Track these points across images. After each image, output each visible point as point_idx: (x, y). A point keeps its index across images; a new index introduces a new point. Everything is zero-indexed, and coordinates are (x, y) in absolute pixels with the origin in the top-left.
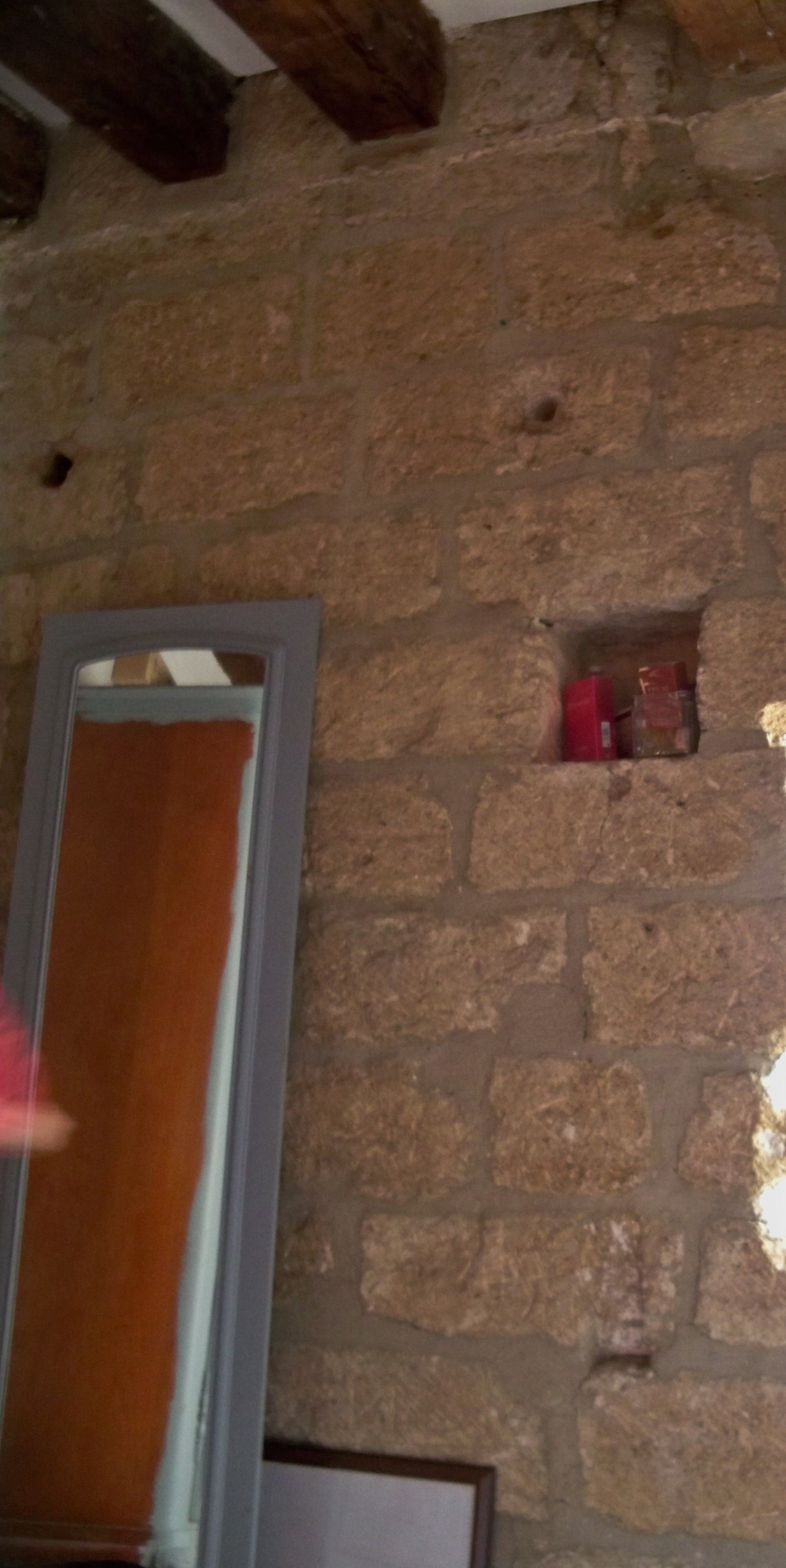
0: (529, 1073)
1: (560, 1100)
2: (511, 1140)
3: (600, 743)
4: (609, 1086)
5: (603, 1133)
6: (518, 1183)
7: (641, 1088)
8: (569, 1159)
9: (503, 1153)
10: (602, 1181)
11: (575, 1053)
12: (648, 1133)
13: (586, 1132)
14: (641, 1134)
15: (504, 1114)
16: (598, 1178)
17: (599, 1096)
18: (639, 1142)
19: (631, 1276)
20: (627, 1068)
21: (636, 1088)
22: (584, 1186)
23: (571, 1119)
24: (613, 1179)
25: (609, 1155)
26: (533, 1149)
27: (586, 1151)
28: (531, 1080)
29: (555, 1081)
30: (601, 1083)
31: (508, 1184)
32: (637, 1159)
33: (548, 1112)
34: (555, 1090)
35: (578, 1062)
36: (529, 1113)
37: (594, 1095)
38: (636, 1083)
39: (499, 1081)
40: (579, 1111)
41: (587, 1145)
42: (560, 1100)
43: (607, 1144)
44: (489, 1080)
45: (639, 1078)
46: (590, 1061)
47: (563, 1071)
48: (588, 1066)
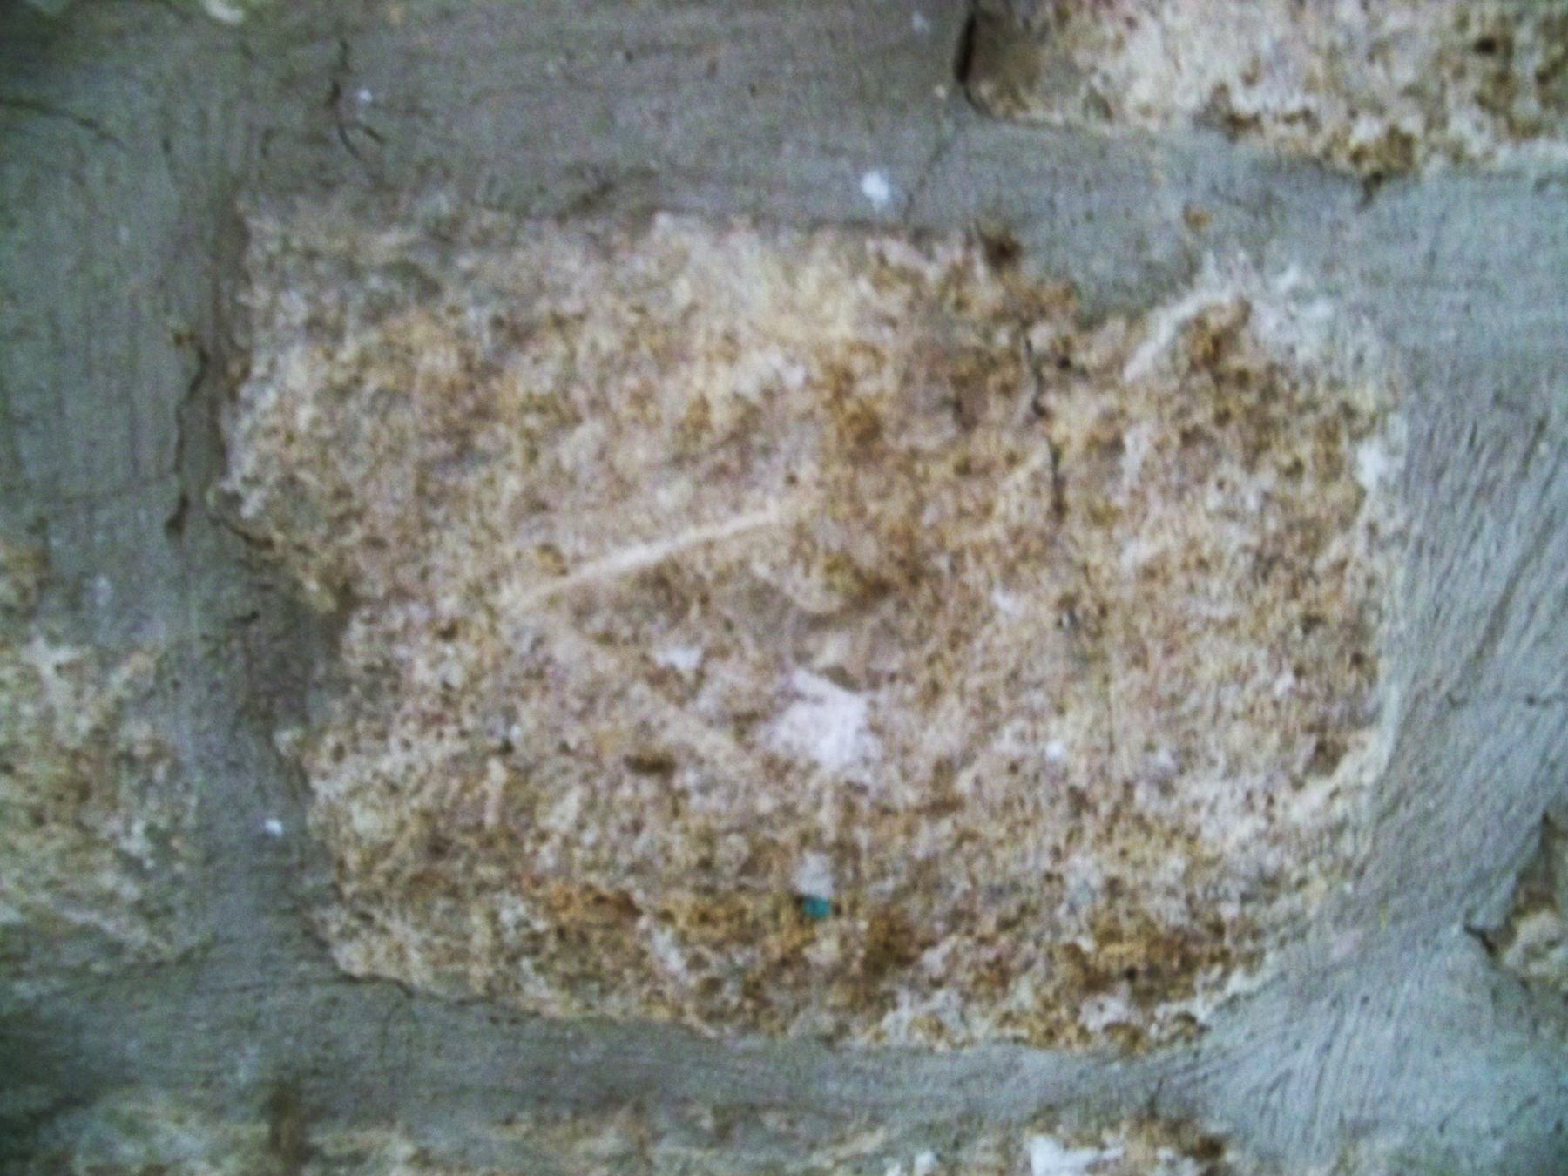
0: (515, 334)
1: (758, 522)
2: (414, 753)
3: (112, 580)
4: (1138, 444)
5: (1060, 744)
6: (479, 972)
7: (1371, 463)
8: (814, 876)
9: (366, 821)
10: (1023, 994)
11: (875, 187)
12: (1369, 756)
13: (943, 733)
14: (1326, 757)
15: (347, 597)
16: (1000, 975)
17: (1059, 509)
18: (1305, 807)
19: (594, 346)
20: (1293, 317)
21: (1333, 468)
22: (904, 1018)
23: (833, 649)
24: (1095, 982)
25: (1086, 868)
26: (562, 814)
27: (932, 836)
28: (531, 376)
29: (721, 386)
30: (1077, 415)
31: (418, 972)
32: (1268, 885)
33: (665, 590)
34: (734, 448)
35: (898, 252)
36: (518, 597)
37: (1015, 498)
38: (1344, 424)
39: (289, 384)
40: (892, 590)
41: (942, 806)
42: (758, 522)
43: (1080, 802)
44: (215, 370)
45: (1366, 398)
46: (1002, 254)
47: (773, 309)
48: (986, 291)
